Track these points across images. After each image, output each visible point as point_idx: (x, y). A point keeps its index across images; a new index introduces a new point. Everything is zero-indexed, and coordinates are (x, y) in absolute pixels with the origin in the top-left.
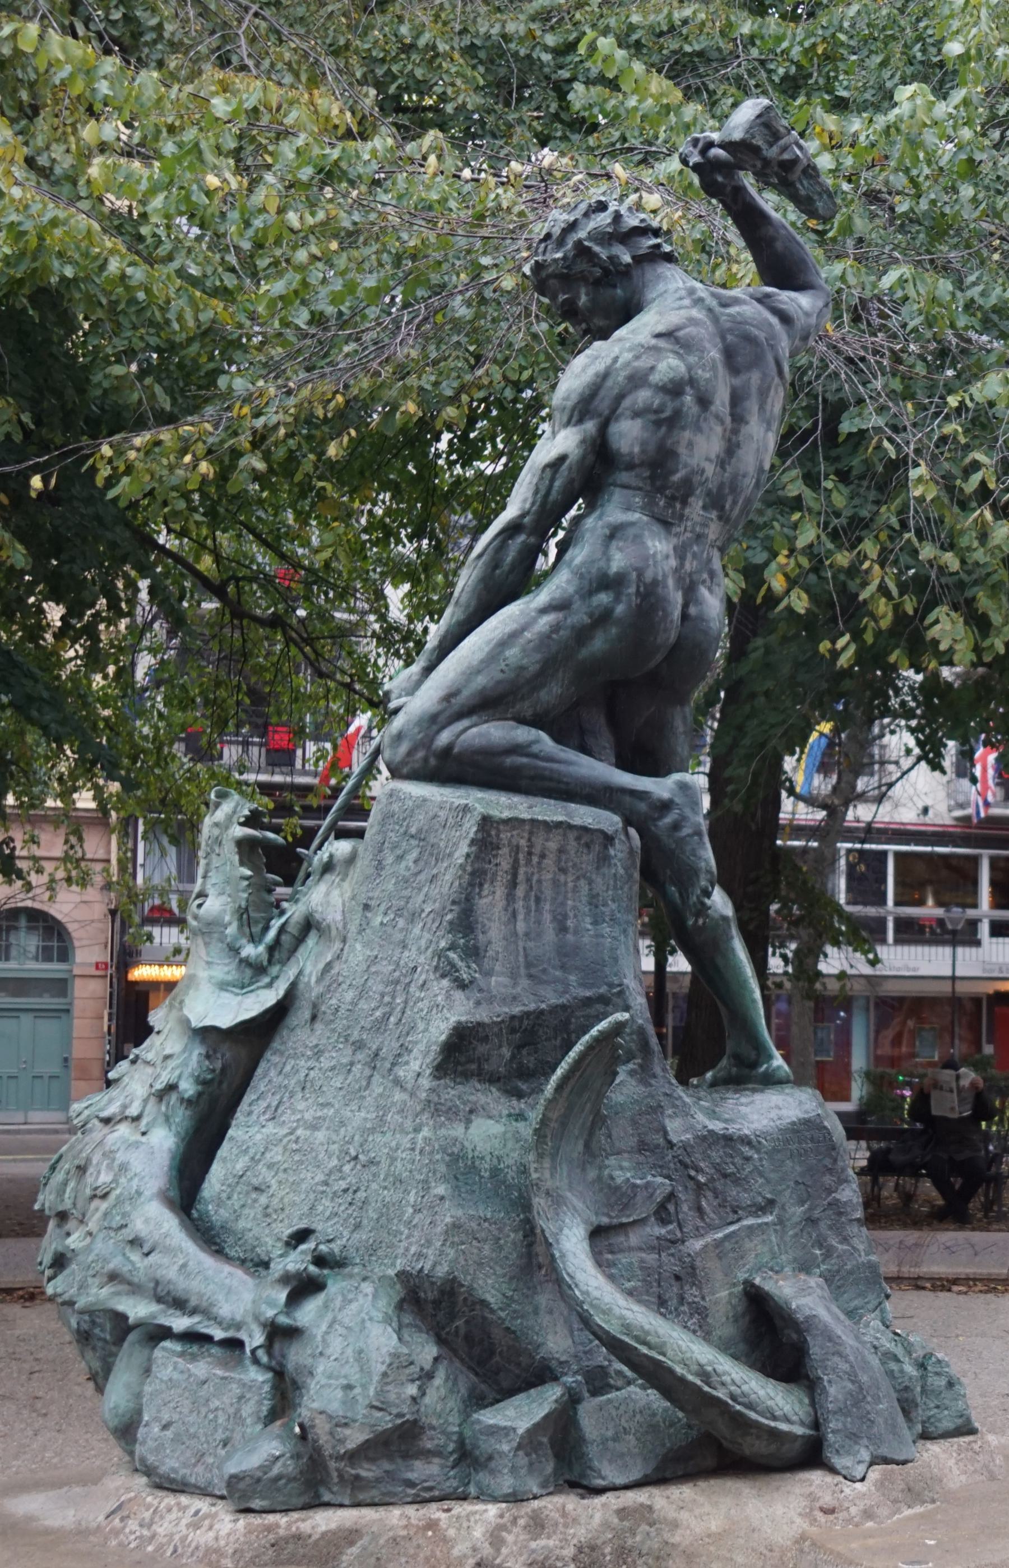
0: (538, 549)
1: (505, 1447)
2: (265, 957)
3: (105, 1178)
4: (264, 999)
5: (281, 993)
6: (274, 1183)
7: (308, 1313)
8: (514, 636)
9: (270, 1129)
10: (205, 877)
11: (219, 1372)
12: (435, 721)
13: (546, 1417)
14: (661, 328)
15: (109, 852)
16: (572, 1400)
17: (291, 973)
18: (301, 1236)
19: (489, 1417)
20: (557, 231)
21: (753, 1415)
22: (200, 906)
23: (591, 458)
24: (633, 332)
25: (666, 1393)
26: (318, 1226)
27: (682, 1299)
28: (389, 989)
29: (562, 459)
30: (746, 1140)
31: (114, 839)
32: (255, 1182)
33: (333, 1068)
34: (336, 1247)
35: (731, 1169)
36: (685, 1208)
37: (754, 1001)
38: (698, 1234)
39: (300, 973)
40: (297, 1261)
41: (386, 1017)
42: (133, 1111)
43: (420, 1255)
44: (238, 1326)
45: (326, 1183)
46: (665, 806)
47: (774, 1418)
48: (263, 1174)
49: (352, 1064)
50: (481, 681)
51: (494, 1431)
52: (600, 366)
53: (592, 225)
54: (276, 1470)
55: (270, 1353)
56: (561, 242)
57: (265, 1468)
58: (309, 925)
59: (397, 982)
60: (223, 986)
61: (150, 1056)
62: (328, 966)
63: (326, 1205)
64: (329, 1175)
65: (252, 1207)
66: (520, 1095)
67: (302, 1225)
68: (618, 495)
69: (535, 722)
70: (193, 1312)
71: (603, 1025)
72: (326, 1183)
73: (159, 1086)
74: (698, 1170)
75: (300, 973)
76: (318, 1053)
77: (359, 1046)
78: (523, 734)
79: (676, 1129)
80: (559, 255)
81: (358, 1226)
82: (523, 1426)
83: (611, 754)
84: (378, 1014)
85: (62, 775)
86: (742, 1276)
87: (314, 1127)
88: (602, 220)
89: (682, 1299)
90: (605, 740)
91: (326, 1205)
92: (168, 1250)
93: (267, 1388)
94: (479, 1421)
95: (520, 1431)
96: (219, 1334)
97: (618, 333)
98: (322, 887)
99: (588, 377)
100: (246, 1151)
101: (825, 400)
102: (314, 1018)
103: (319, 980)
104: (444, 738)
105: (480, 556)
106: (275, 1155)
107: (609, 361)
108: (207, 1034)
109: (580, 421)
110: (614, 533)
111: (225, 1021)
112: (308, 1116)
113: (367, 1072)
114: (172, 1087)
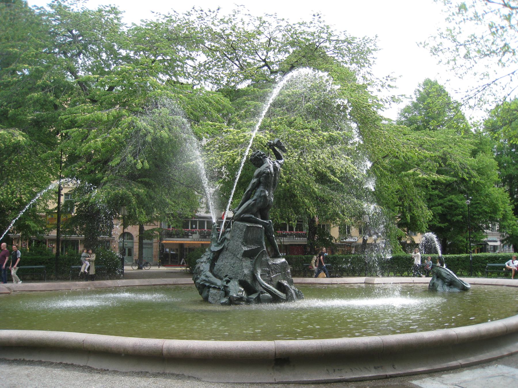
0: (251, 194)
4: (221, 247)
7: (229, 285)
8: (250, 204)
12: (241, 214)
16: (259, 295)
17: (223, 245)
18: (226, 276)
19: (250, 297)
29: (255, 182)
30: (277, 264)
37: (129, 298)
38: (272, 275)
40: (227, 278)
42: (205, 261)
44: (220, 286)
46: (268, 224)
52: (259, 171)
56: (254, 156)
57: (225, 302)
58: (423, 183)
60: (215, 246)
63: (229, 272)
66: (252, 259)
68: (262, 187)
69: (252, 214)
76: (227, 254)
77: (232, 253)
82: (254, 297)
85: (418, 175)
87: (227, 263)
88: (259, 153)
90: (259, 216)
91: (229, 272)
96: (217, 287)
99: (258, 173)
101: (34, 205)
104: (242, 216)
106: (222, 266)
108: (214, 252)
110: (261, 191)
114: (209, 258)
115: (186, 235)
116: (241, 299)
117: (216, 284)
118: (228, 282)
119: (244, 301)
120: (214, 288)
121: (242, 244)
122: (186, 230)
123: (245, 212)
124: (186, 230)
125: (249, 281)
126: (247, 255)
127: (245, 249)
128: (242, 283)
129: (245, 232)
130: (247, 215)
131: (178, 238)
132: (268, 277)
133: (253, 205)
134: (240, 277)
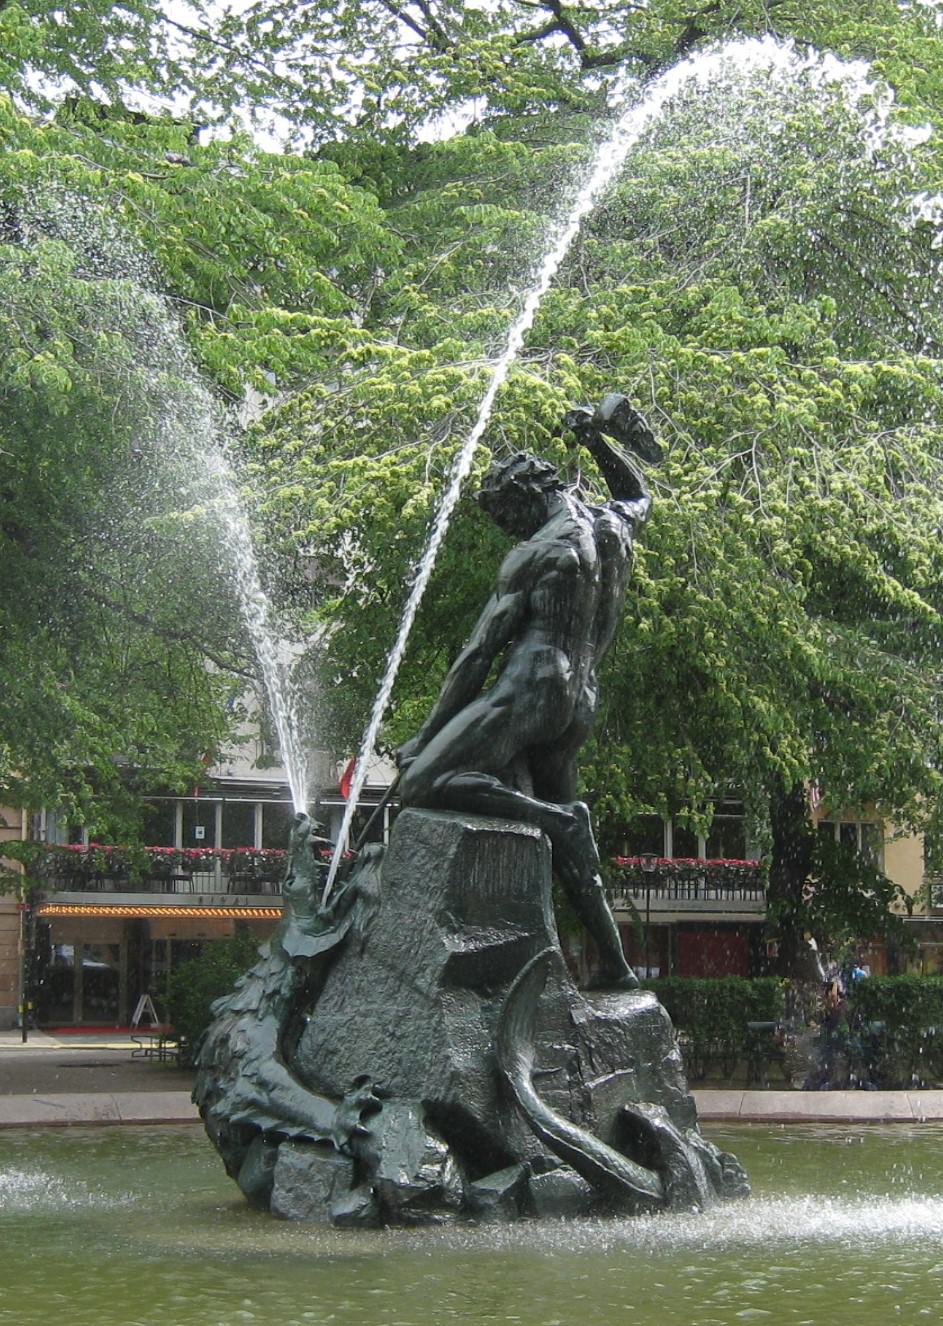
1: (491, 1201)
2: (331, 915)
3: (240, 1046)
4: (334, 938)
5: (342, 936)
6: (342, 1049)
7: (374, 1125)
8: (478, 720)
9: (338, 1017)
10: (720, 912)
11: (321, 1159)
12: (433, 771)
13: (513, 1185)
14: (561, 533)
15: (20, 821)
17: (347, 924)
19: (480, 1185)
20: (496, 474)
21: (631, 1185)
22: (291, 884)
23: (521, 612)
24: (544, 536)
25: (582, 1172)
26: (372, 1075)
27: (584, 1119)
28: (410, 933)
29: (504, 613)
31: (24, 813)
32: (331, 1048)
33: (375, 981)
34: (384, 1086)
35: (609, 1040)
36: (583, 1063)
38: (592, 1078)
39: (353, 925)
41: (408, 950)
42: (253, 1006)
43: (436, 1090)
45: (375, 1049)
46: (567, 821)
47: (643, 1188)
48: (334, 1043)
49: (388, 978)
50: (460, 748)
51: (485, 1192)
52: (526, 557)
53: (517, 471)
54: (364, 1213)
55: (350, 1146)
57: (356, 1212)
59: (415, 930)
61: (259, 974)
62: (370, 920)
63: (376, 1062)
64: (377, 1043)
65: (329, 1063)
67: (362, 1073)
70: (300, 1125)
71: (541, 954)
72: (375, 1049)
73: (268, 991)
74: (591, 1041)
75: (353, 925)
76: (365, 971)
77: (392, 967)
78: (486, 779)
79: (580, 1018)
80: (498, 489)
81: (395, 1075)
82: (501, 1189)
83: (532, 793)
84: (403, 948)
86: (617, 1104)
87: (365, 1015)
88: (523, 467)
89: (584, 1119)
90: (527, 782)
91: (376, 1062)
92: (283, 1088)
93: (350, 1167)
94: (474, 1187)
95: (501, 1192)
96: (317, 1137)
97: (537, 536)
98: (364, 872)
100: (323, 1030)
102: (362, 951)
103: (365, 929)
104: (438, 782)
105: (455, 673)
107: (530, 555)
108: (298, 961)
109: (515, 591)
111: (309, 953)
112: (362, 1008)
113: (398, 983)
115: (160, 878)
116: (432, 1198)
117: (308, 1123)
118: (369, 1110)
119: (449, 1207)
120: (301, 1141)
121: (442, 920)
122: (160, 853)
123: (457, 757)
124: (160, 853)
125: (476, 1107)
126: (462, 975)
127: (456, 944)
128: (441, 1118)
129: (455, 863)
130: (464, 779)
131: (119, 889)
132: (570, 1086)
133: (497, 727)
134: (432, 1088)
